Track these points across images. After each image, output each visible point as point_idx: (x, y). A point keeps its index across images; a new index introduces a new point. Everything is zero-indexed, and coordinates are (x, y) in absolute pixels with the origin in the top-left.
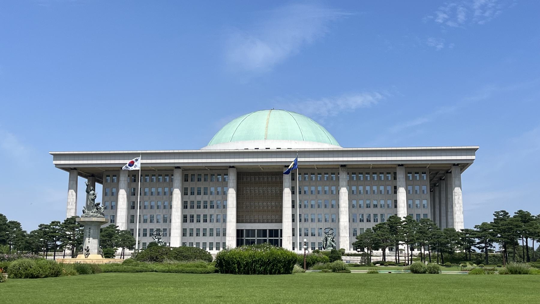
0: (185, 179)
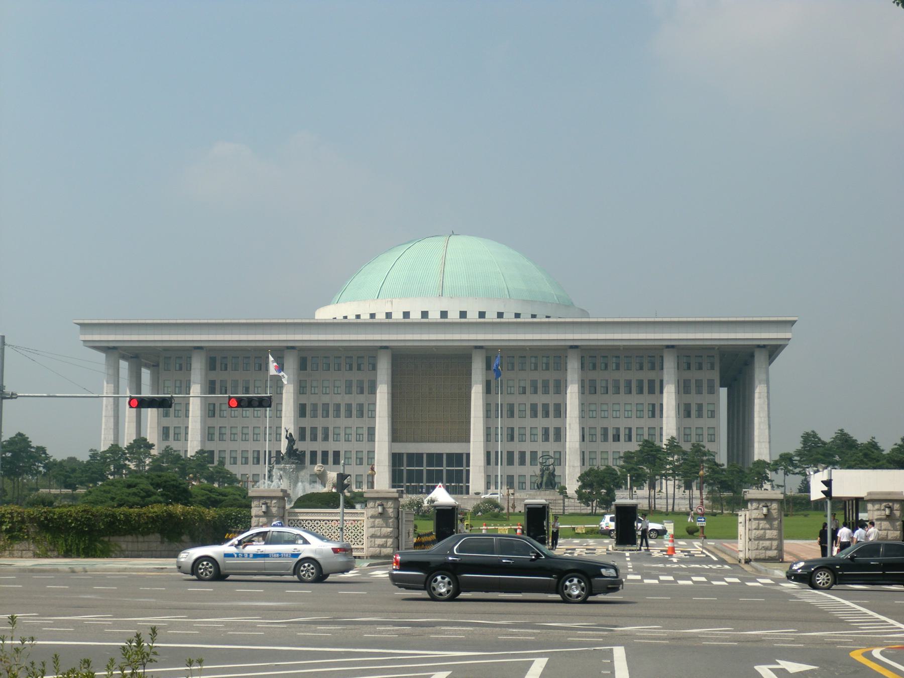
0: (212, 365)
